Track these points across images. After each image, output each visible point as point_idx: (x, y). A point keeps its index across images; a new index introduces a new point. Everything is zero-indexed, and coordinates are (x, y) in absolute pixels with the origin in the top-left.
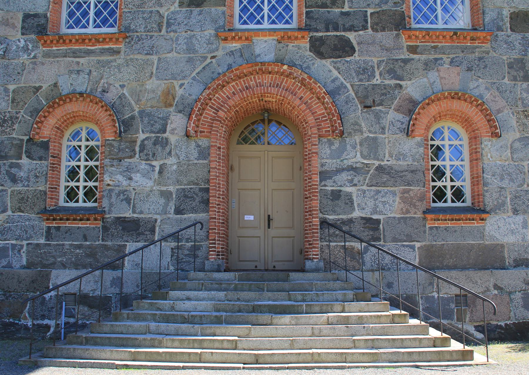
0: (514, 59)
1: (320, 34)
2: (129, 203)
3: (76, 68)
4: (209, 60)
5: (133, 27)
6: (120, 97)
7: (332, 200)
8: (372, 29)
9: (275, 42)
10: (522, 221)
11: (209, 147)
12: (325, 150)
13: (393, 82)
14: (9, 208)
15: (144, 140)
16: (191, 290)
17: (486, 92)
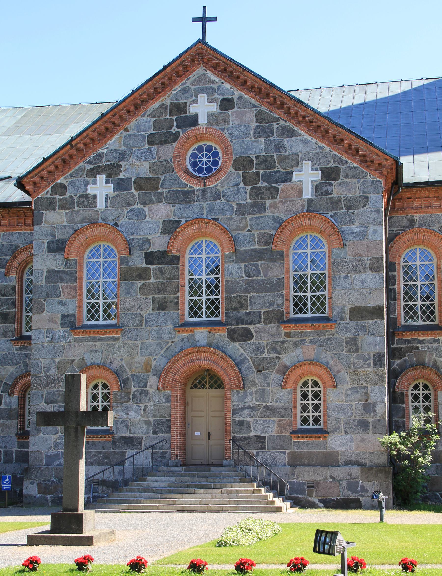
0: (350, 338)
1: (233, 327)
2: (127, 428)
3: (94, 349)
4: (170, 344)
5: (126, 323)
6: (120, 366)
7: (239, 426)
8: (264, 322)
9: (207, 333)
10: (350, 438)
11: (171, 396)
12: (235, 397)
13: (275, 355)
14: (59, 431)
15: (135, 392)
16: (159, 477)
17: (331, 360)
